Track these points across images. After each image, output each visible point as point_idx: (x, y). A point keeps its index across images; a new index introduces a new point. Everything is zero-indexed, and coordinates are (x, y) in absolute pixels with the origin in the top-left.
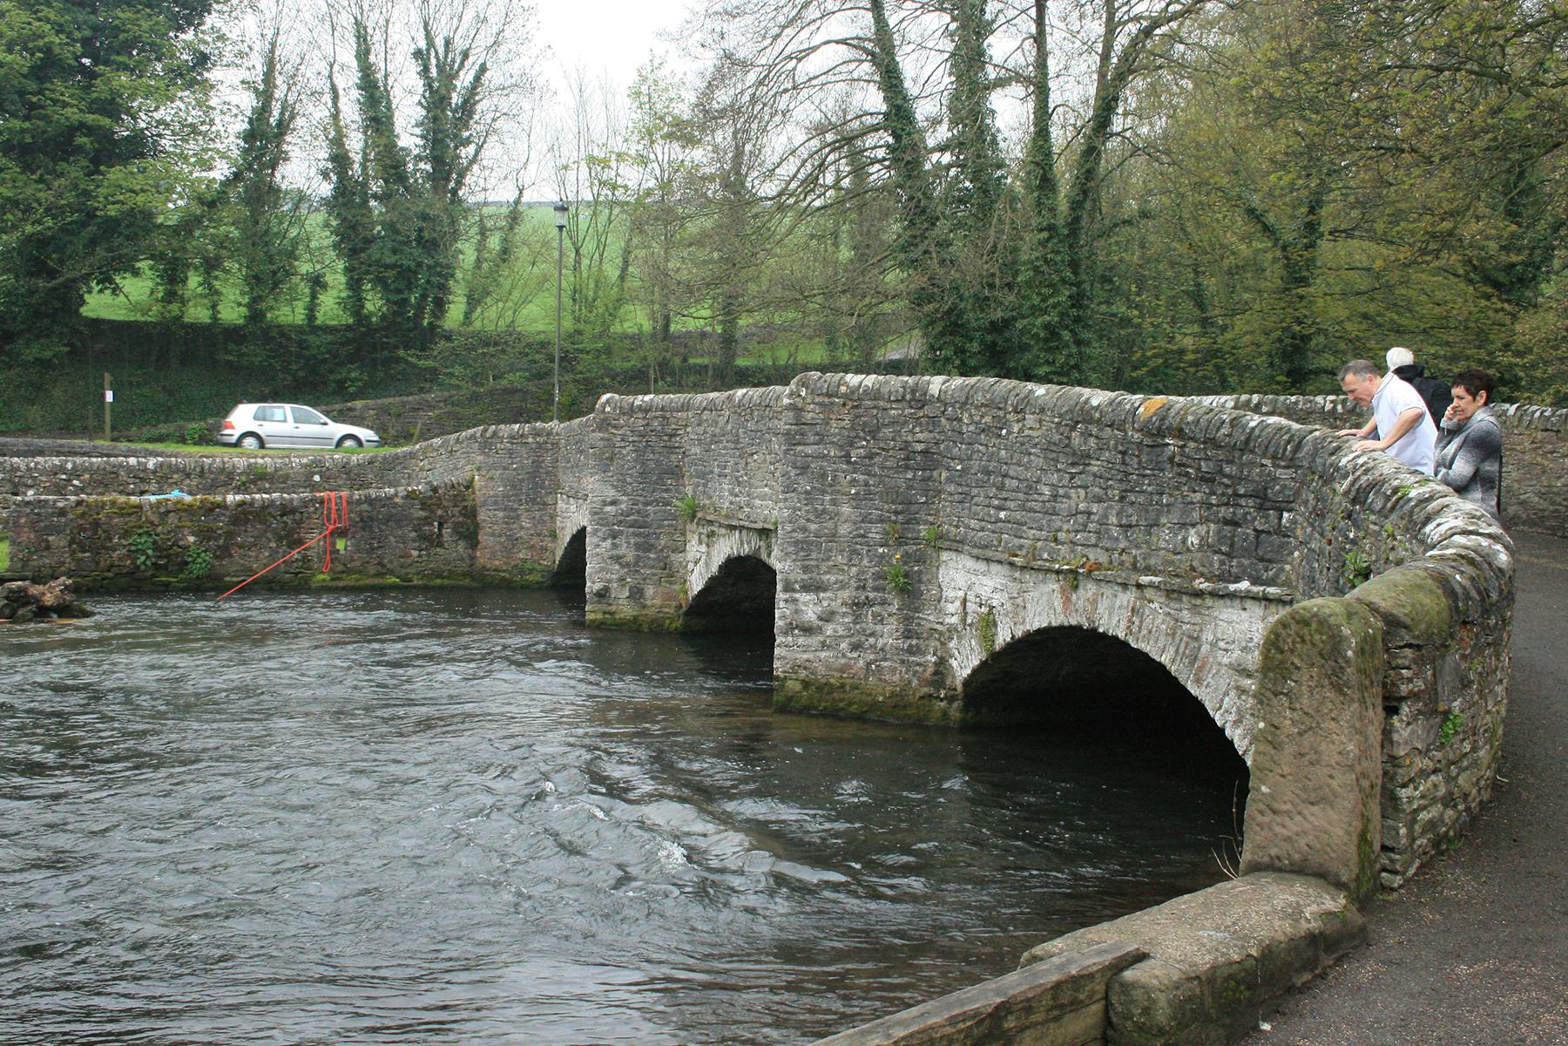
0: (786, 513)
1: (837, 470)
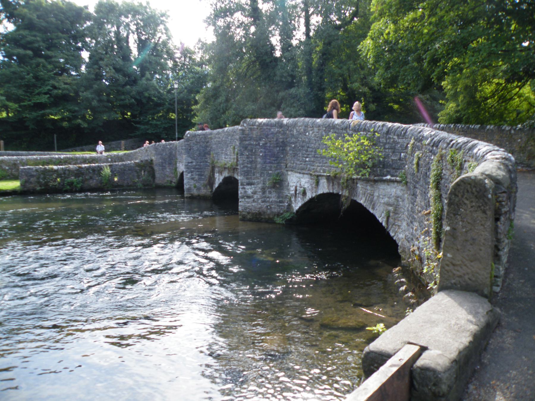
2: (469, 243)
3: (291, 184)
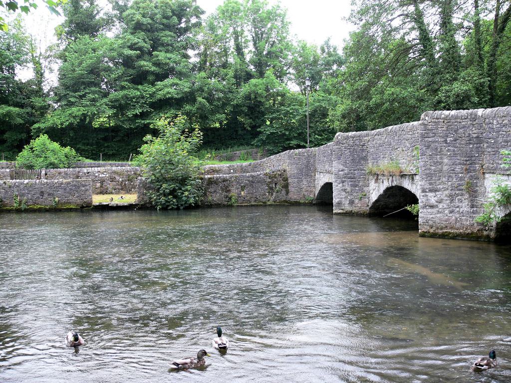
0: (422, 163)
1: (442, 146)
3: (489, 190)
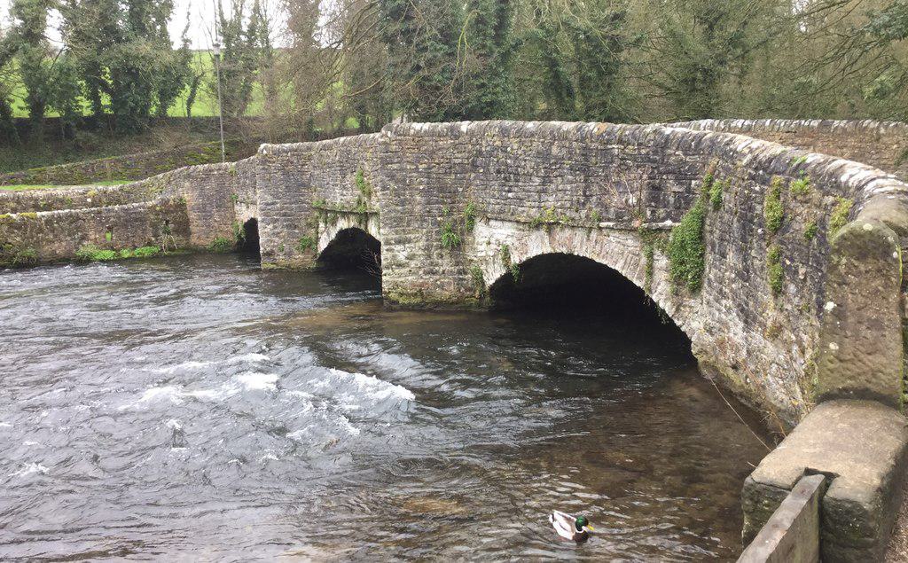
2: (864, 327)
